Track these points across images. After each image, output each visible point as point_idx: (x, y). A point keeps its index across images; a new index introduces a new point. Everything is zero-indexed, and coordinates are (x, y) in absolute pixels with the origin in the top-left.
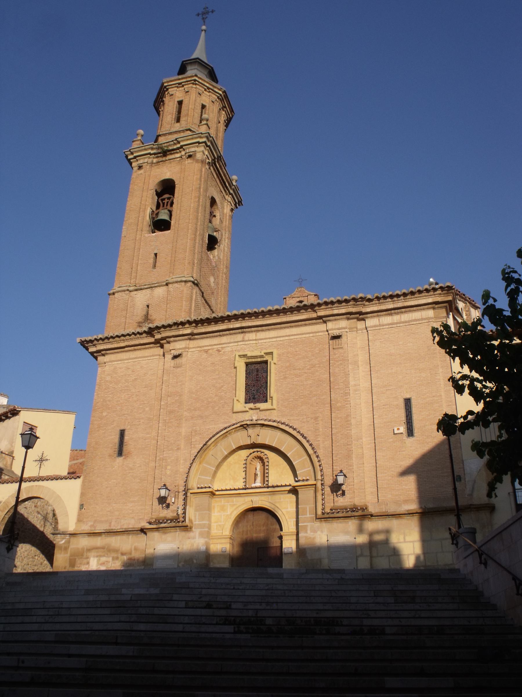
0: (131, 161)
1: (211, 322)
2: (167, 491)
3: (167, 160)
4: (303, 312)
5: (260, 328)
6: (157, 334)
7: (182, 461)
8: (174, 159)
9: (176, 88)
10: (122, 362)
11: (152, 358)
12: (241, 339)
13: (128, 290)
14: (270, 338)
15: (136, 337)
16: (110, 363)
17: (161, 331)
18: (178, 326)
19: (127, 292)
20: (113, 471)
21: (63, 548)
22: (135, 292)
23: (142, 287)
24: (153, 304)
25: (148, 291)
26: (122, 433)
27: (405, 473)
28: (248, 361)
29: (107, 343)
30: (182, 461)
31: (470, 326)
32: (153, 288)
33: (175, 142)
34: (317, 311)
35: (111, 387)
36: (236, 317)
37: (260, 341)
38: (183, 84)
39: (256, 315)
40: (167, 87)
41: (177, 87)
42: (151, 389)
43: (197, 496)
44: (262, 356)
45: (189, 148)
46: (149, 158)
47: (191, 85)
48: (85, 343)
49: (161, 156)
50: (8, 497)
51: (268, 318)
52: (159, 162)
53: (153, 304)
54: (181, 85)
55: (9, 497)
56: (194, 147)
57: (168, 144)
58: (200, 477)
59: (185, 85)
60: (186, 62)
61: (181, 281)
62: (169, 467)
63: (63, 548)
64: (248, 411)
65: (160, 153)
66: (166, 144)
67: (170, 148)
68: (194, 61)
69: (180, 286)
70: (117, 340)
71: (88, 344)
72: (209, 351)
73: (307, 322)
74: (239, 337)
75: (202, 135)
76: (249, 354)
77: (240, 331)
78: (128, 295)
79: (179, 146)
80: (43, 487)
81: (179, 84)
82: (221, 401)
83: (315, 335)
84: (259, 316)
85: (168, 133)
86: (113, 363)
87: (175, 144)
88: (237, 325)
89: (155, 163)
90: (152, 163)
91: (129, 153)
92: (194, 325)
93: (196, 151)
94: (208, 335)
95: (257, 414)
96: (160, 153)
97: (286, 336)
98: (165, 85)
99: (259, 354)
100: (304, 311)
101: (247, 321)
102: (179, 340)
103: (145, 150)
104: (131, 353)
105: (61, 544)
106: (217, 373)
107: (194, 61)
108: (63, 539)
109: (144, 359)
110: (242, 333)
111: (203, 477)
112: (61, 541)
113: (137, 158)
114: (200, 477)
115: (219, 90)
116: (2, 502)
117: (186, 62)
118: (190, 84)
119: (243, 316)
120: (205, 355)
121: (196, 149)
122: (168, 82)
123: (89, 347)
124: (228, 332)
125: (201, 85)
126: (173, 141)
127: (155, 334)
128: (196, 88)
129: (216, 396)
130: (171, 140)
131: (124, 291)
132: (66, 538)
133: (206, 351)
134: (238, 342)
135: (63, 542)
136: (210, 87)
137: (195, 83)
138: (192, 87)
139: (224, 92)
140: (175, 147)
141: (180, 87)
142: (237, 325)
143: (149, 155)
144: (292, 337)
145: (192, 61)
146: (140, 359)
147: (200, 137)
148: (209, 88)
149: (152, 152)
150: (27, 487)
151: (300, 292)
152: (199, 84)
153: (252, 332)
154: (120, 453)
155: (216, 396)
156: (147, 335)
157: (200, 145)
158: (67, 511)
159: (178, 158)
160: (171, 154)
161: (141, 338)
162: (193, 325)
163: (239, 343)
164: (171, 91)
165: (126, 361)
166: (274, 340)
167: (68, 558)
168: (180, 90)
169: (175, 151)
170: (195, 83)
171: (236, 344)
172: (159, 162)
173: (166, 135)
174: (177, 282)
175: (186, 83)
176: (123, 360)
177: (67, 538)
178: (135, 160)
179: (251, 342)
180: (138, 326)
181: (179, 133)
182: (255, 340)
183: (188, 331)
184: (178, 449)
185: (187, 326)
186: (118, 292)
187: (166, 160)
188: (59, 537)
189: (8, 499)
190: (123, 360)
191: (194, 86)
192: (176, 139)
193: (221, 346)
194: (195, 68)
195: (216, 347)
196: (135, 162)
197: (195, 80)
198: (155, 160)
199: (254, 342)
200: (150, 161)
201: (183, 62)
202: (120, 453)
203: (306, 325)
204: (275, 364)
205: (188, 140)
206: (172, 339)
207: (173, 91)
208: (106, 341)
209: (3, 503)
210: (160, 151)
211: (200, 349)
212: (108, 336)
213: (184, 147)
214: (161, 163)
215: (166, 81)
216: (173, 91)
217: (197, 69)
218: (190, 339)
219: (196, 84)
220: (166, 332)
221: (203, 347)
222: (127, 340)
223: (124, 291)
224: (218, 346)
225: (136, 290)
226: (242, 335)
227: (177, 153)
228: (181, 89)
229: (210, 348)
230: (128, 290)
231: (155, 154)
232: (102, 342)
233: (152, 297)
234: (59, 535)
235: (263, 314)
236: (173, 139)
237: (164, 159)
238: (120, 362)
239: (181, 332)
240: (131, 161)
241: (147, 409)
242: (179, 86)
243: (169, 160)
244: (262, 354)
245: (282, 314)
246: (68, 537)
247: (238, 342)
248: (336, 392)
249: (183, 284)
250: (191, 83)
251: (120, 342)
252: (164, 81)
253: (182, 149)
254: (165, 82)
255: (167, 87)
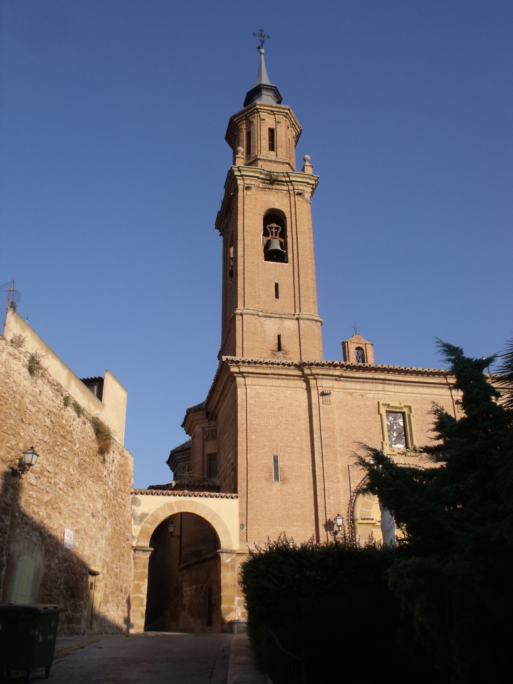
0: (237, 177)
1: (360, 369)
2: (35, 456)
3: (274, 189)
4: (437, 377)
5: (399, 383)
6: (307, 369)
7: (342, 493)
8: (281, 190)
9: (267, 114)
10: (265, 387)
11: (295, 389)
12: (382, 389)
13: (258, 315)
14: (405, 393)
15: (284, 367)
16: (251, 387)
17: (312, 368)
18: (330, 367)
19: (256, 317)
20: (272, 495)
21: (229, 567)
22: (264, 319)
23: (272, 315)
24: (284, 335)
25: (278, 320)
26: (276, 459)
27: (220, 236)
28: (388, 409)
29: (252, 366)
30: (342, 493)
31: (492, 396)
32: (283, 319)
33: (285, 175)
34: (447, 378)
35: (256, 410)
36: (383, 370)
37: (398, 394)
38: (275, 112)
39: (400, 371)
40: (259, 110)
41: (269, 113)
42: (299, 420)
43: (362, 526)
44: (401, 408)
45: (297, 185)
46: (256, 181)
47: (282, 117)
48: (229, 363)
49: (267, 183)
50: (155, 510)
51: (408, 376)
52: (265, 188)
53: (284, 335)
54: (273, 113)
55: (157, 510)
56: (303, 186)
57: (278, 174)
58: (362, 509)
59: (277, 114)
60: (264, 86)
61: (313, 320)
62: (332, 497)
63: (229, 567)
64: (396, 455)
65: (267, 180)
66: (275, 174)
67: (280, 179)
68: (271, 88)
69: (311, 324)
70: (264, 366)
71: (231, 363)
72: (353, 394)
73: (437, 385)
74: (380, 387)
75: (312, 178)
76: (392, 404)
77: (382, 381)
78: (258, 319)
79: (288, 179)
80: (197, 503)
81: (271, 111)
82: (371, 442)
83: (441, 397)
84: (402, 372)
85: (268, 160)
86: (255, 387)
87: (284, 176)
88: (382, 376)
89: (261, 188)
90: (259, 187)
91: (237, 169)
92: (345, 368)
93: (304, 190)
94: (353, 380)
95: (403, 458)
96: (267, 180)
97: (420, 394)
98: (258, 107)
99: (397, 405)
100: (438, 376)
101: (390, 375)
102: (326, 379)
103: (254, 172)
104: (274, 381)
105: (226, 562)
106: (363, 416)
107: (271, 88)
108: (229, 557)
109: (287, 389)
110: (382, 383)
111: (364, 509)
112: (227, 559)
113: (244, 177)
114: (362, 509)
115: (299, 128)
116: (149, 513)
117: (264, 86)
118: (281, 115)
119: (389, 371)
120: (349, 397)
121: (305, 188)
122: (260, 105)
123: (231, 367)
124: (371, 381)
125: (289, 119)
126: (283, 173)
127: (304, 369)
128: (286, 121)
129: (366, 437)
130: (282, 172)
131: (254, 315)
132: (232, 557)
133: (351, 394)
134: (379, 391)
135: (229, 560)
136: (294, 123)
137: (286, 115)
138: (283, 119)
139: (301, 131)
140: (284, 179)
141: (271, 114)
142: (382, 376)
143: (257, 179)
144: (424, 396)
145: (269, 87)
146: (283, 389)
147: (311, 179)
148: (293, 124)
149: (261, 176)
150: (178, 501)
151: (357, 338)
152: (289, 118)
153: (391, 384)
154: (277, 478)
155: (366, 437)
156: (296, 368)
157: (308, 185)
158: (228, 530)
159: (284, 190)
160: (278, 184)
161: (288, 369)
162: (343, 369)
163: (380, 392)
164: (263, 115)
165: (268, 388)
166: (409, 395)
167: (236, 577)
168: (270, 117)
169: (283, 183)
170: (286, 115)
171: (377, 392)
172: (265, 188)
173: (266, 161)
174: (308, 319)
175: (279, 113)
176: (265, 386)
177: (233, 556)
178: (241, 178)
179: (391, 393)
180: (272, 354)
181: (279, 163)
182: (394, 392)
183: (338, 373)
184: (339, 481)
185: (338, 368)
186: (247, 314)
187: (273, 189)
188: (224, 556)
189: (156, 511)
190: (265, 386)
191: (284, 118)
192: (287, 173)
193: (363, 391)
194: (270, 94)
195: (359, 391)
196: (240, 179)
197: (287, 114)
198: (261, 185)
199: (393, 394)
200: (257, 184)
201: (261, 85)
202: (277, 478)
203: (435, 387)
204: (413, 416)
205: (298, 177)
206: (320, 377)
207: (265, 116)
208: (252, 365)
209: (151, 515)
210: (268, 178)
211: (345, 390)
212: (257, 361)
213: (293, 182)
214: (267, 189)
215: (259, 103)
216: (265, 116)
217: (271, 97)
218: (336, 380)
219: (286, 117)
220: (316, 369)
221: (348, 389)
222: (274, 368)
223: (254, 315)
224: (361, 391)
225: (265, 317)
226: (382, 385)
227: (284, 185)
228: (271, 116)
229: (354, 391)
230: (258, 315)
231: (262, 179)
232: (247, 365)
233: (282, 328)
234: (225, 554)
235: (406, 372)
236: (284, 172)
237: (270, 186)
238: (261, 387)
239: (331, 373)
240: (237, 177)
241: (298, 439)
242: (271, 113)
243: (275, 189)
244: (402, 406)
245: (420, 375)
246: (234, 556)
247: (379, 391)
248: (374, 426)
249: (314, 322)
250: (283, 115)
251: (266, 368)
252: (257, 103)
253: (290, 184)
254: (258, 105)
255: (259, 110)
